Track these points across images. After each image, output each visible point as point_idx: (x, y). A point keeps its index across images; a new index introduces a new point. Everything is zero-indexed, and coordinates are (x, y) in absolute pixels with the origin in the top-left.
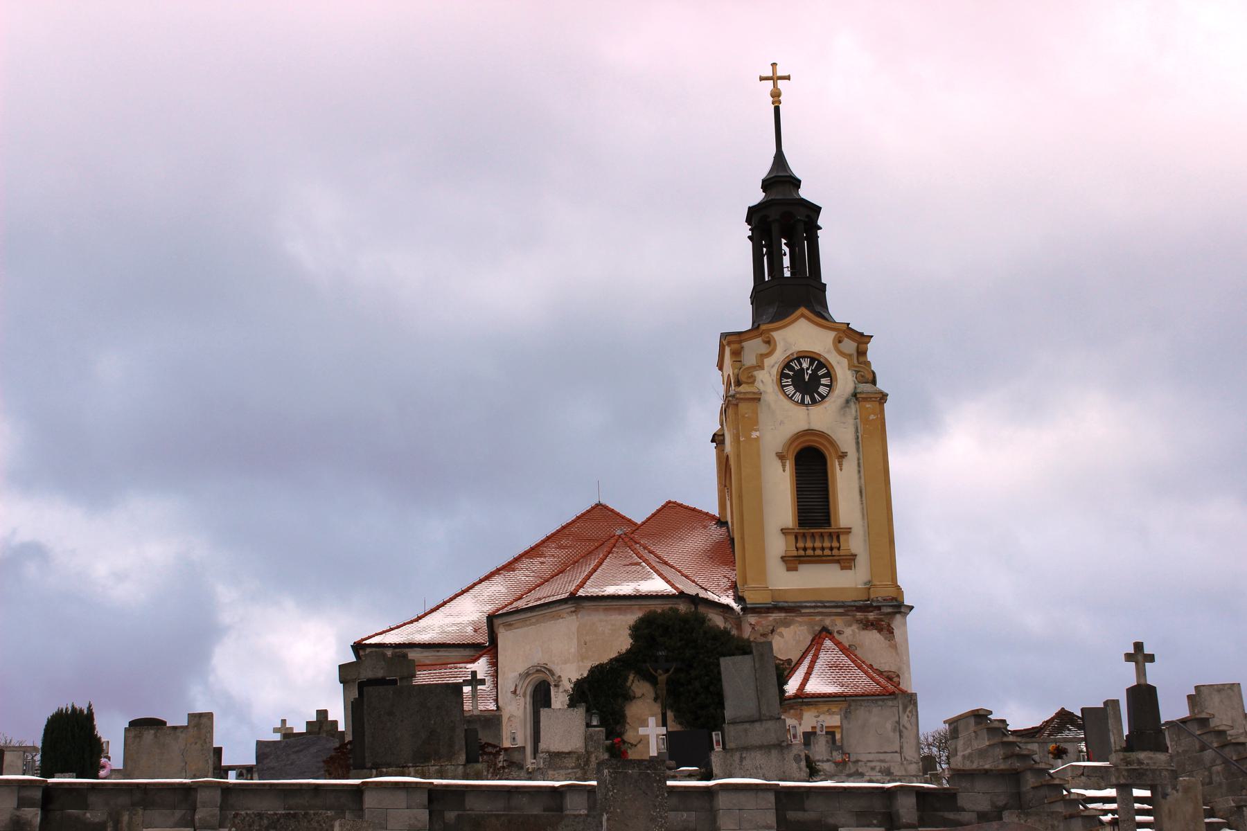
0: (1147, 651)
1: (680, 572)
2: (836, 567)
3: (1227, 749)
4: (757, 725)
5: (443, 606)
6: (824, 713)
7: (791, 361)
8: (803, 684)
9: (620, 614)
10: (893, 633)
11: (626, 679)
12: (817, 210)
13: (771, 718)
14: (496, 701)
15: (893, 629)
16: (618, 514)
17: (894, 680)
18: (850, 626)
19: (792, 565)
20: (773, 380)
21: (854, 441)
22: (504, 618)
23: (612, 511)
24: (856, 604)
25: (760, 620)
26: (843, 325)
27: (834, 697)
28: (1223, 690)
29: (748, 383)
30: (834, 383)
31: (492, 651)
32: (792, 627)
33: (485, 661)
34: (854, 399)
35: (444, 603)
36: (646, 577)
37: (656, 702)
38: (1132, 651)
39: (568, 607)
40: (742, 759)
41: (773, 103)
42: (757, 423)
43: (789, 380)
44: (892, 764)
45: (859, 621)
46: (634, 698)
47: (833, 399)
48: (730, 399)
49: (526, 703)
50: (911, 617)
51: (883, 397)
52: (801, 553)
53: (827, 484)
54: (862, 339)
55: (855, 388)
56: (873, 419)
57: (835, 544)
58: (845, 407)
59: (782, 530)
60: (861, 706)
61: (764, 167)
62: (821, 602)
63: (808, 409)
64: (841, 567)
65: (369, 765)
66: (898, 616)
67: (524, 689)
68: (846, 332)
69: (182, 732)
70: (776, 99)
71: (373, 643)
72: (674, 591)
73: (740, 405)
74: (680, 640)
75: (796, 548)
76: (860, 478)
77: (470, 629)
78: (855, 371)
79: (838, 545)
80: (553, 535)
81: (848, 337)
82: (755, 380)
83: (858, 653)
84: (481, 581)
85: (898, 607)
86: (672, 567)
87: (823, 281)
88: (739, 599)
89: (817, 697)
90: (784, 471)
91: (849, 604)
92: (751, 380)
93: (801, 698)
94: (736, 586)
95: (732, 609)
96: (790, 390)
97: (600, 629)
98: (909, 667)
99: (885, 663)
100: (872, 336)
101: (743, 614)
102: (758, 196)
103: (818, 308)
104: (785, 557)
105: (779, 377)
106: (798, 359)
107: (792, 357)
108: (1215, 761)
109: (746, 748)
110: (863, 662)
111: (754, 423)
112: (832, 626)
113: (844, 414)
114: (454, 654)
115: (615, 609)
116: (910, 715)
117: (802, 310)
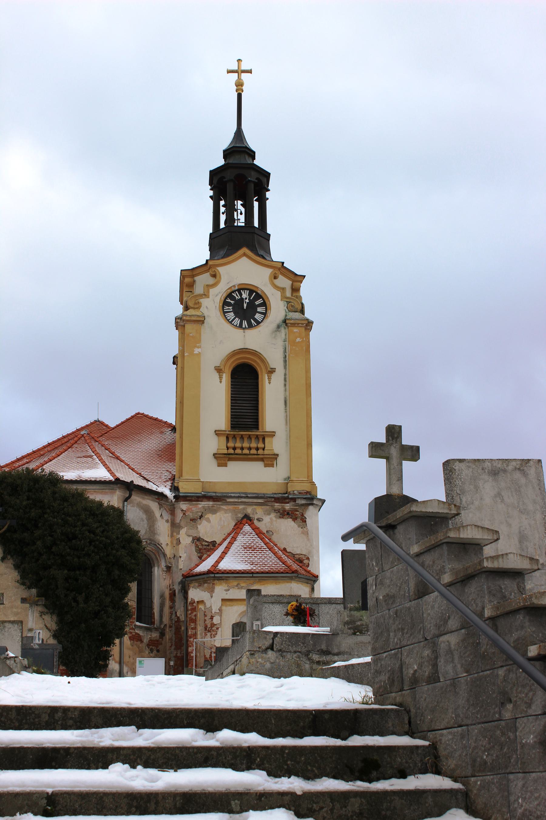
0: (407, 440)
1: (128, 465)
2: (260, 464)
3: (472, 588)
6: (233, 588)
7: (233, 292)
8: (218, 562)
10: (305, 521)
15: (306, 518)
17: (305, 562)
18: (269, 514)
19: (223, 462)
20: (216, 307)
21: (283, 359)
24: (275, 496)
25: (191, 507)
27: (243, 573)
28: (505, 471)
29: (194, 308)
30: (268, 311)
32: (218, 514)
41: (236, 91)
42: (199, 341)
43: (230, 308)
45: (277, 511)
51: (309, 324)
52: (231, 451)
53: (257, 395)
55: (286, 316)
56: (299, 342)
57: (261, 445)
58: (276, 331)
62: (244, 493)
63: (244, 332)
66: (311, 507)
70: (240, 87)
72: (112, 478)
73: (186, 325)
76: (285, 390)
78: (287, 302)
79: (263, 446)
82: (201, 306)
83: (274, 538)
87: (268, 232)
88: (175, 489)
89: (228, 573)
90: (221, 382)
92: (196, 306)
93: (213, 573)
94: (174, 478)
95: (166, 496)
96: (231, 316)
100: (304, 276)
101: (175, 502)
103: (261, 252)
104: (216, 454)
105: (221, 304)
106: (239, 290)
107: (233, 289)
108: (446, 621)
110: (276, 545)
113: (275, 337)
117: (245, 250)
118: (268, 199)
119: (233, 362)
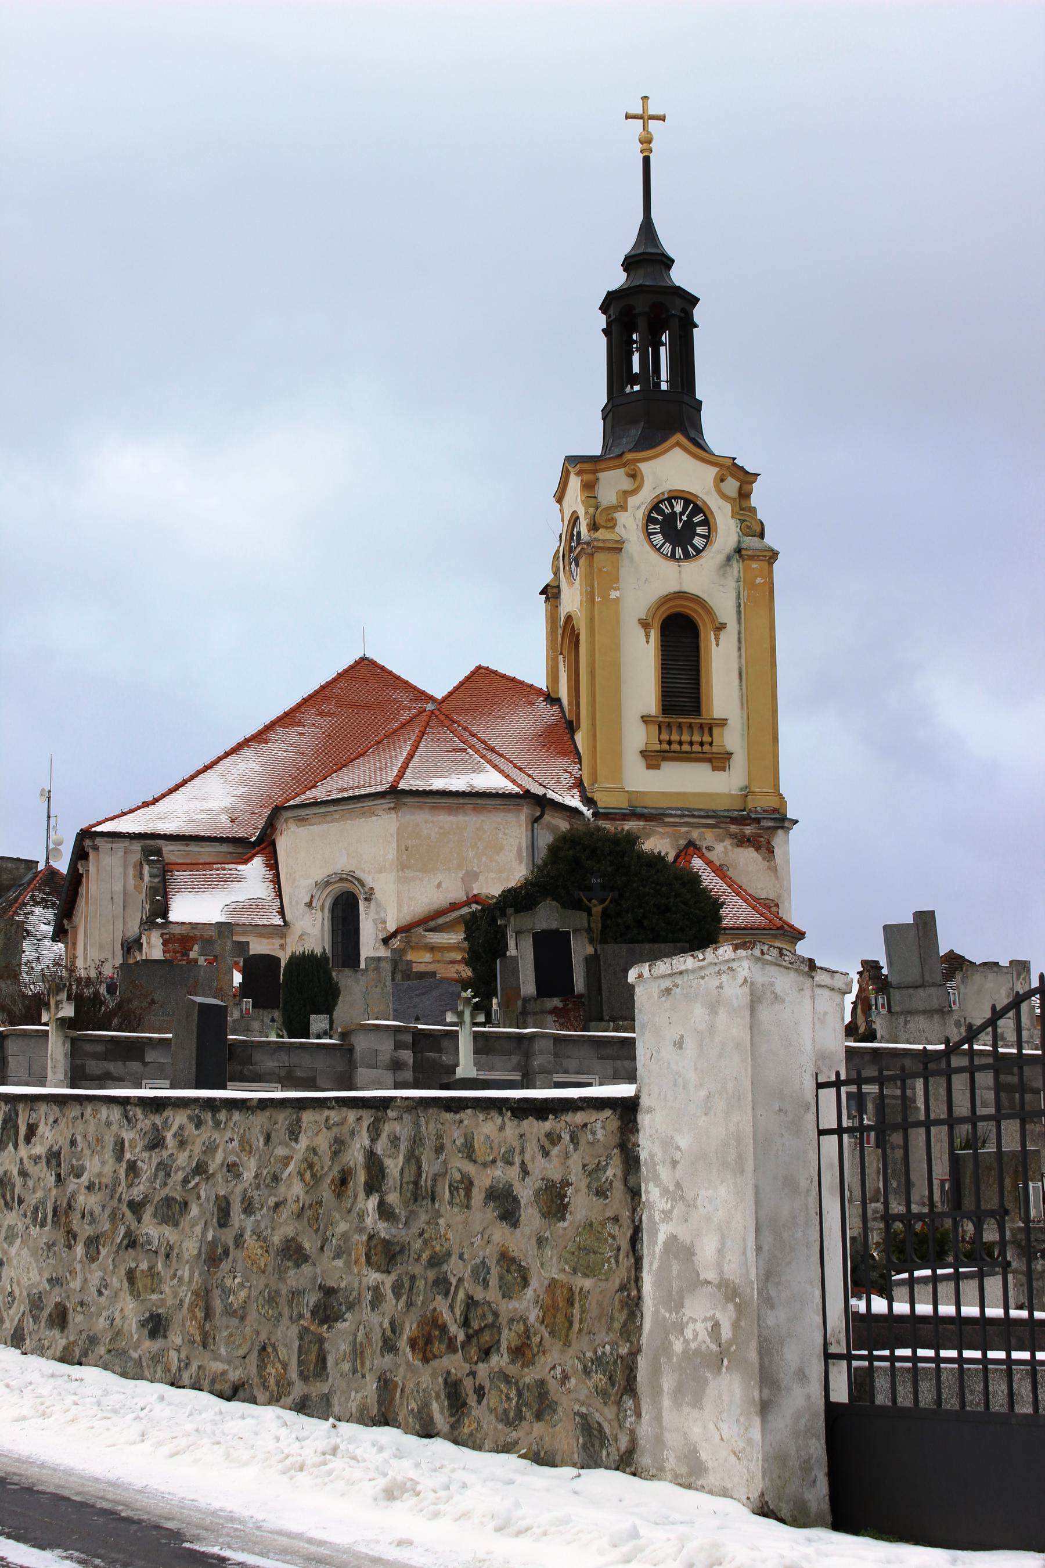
2: (706, 767)
4: (921, 991)
5: (183, 785)
7: (661, 502)
9: (449, 815)
12: (694, 301)
13: (934, 985)
14: (282, 912)
16: (390, 673)
18: (722, 841)
19: (654, 762)
23: (382, 668)
24: (730, 814)
29: (606, 528)
30: (713, 534)
31: (267, 850)
33: (261, 862)
34: (737, 556)
35: (185, 782)
36: (478, 770)
39: (387, 803)
40: (906, 1023)
42: (617, 579)
43: (657, 527)
44: (1005, 1030)
45: (733, 836)
47: (711, 555)
48: (585, 546)
49: (323, 919)
50: (795, 832)
52: (666, 747)
54: (746, 478)
55: (739, 541)
57: (707, 739)
59: (642, 717)
60: (977, 971)
61: (627, 241)
62: (687, 809)
65: (607, 1018)
66: (780, 832)
67: (321, 901)
69: (362, 975)
70: (645, 146)
71: (106, 830)
72: (517, 790)
73: (595, 555)
75: (659, 740)
76: (740, 656)
77: (224, 818)
79: (710, 739)
80: (311, 697)
81: (733, 475)
82: (615, 525)
84: (227, 755)
85: (782, 822)
88: (589, 801)
90: (648, 642)
91: (721, 814)
92: (610, 524)
95: (581, 813)
96: (658, 539)
97: (426, 831)
98: (789, 895)
99: (762, 889)
100: (759, 475)
102: (618, 279)
105: (644, 522)
106: (669, 500)
107: (662, 497)
109: (910, 1013)
110: (740, 887)
111: (613, 579)
112: (700, 839)
114: (207, 852)
115: (443, 808)
116: (1023, 982)
117: (679, 437)
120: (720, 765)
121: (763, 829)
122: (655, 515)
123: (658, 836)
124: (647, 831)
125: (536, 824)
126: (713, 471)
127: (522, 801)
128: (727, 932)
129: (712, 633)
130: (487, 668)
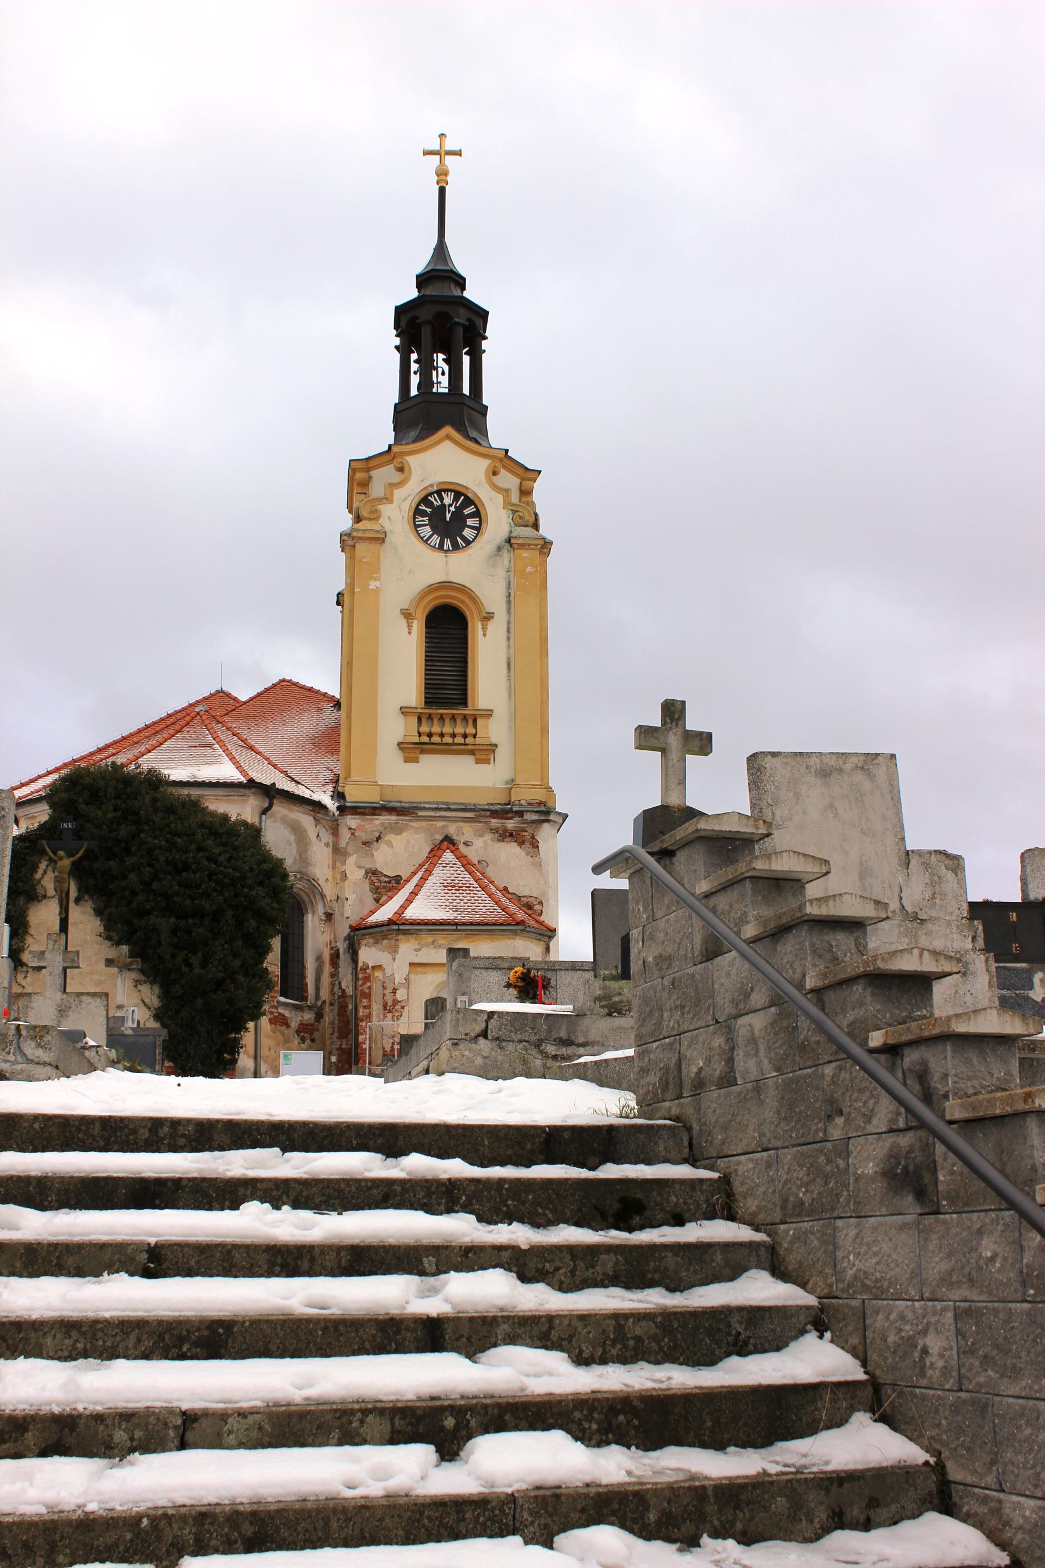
0: (693, 723)
1: (267, 759)
2: (469, 759)
3: (788, 946)
7: (430, 494)
8: (404, 907)
10: (537, 847)
11: (35, 868)
18: (482, 835)
19: (412, 755)
22: (25, 809)
24: (492, 808)
25: (363, 823)
26: (499, 452)
28: (840, 771)
29: (369, 519)
30: (484, 525)
32: (404, 834)
37: (77, 904)
38: (657, 722)
41: (438, 184)
43: (425, 519)
46: (45, 897)
52: (425, 739)
53: (466, 653)
54: (528, 475)
55: (511, 532)
57: (470, 730)
58: (495, 556)
61: (421, 260)
64: (476, 759)
68: (505, 460)
73: (358, 546)
74: (115, 810)
75: (419, 733)
76: (509, 647)
79: (474, 731)
83: (489, 872)
86: (258, 753)
88: (338, 796)
89: (419, 924)
90: (410, 633)
91: (481, 807)
94: (338, 780)
96: (426, 531)
100: (540, 472)
101: (339, 815)
105: (411, 514)
106: (439, 492)
107: (430, 490)
108: (747, 995)
110: (492, 882)
117: (448, 430)
118: (484, 351)
119: (428, 604)
120: (484, 757)
121: (527, 823)
122: (424, 508)
123: (411, 831)
124: (400, 826)
125: (264, 816)
126: (484, 464)
127: (247, 791)
128: (459, 927)
129: (480, 623)
130: (290, 681)
